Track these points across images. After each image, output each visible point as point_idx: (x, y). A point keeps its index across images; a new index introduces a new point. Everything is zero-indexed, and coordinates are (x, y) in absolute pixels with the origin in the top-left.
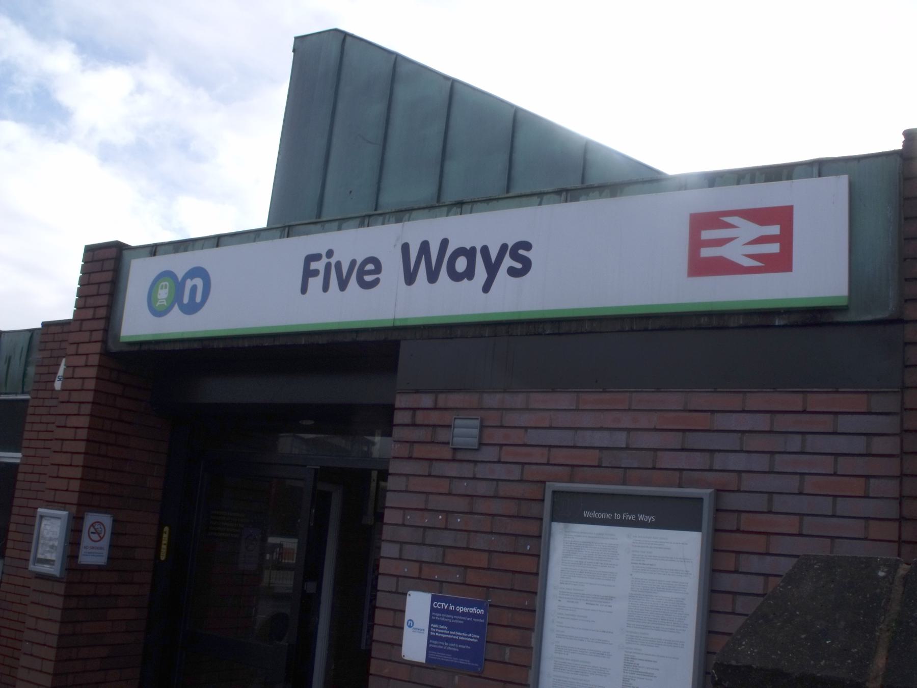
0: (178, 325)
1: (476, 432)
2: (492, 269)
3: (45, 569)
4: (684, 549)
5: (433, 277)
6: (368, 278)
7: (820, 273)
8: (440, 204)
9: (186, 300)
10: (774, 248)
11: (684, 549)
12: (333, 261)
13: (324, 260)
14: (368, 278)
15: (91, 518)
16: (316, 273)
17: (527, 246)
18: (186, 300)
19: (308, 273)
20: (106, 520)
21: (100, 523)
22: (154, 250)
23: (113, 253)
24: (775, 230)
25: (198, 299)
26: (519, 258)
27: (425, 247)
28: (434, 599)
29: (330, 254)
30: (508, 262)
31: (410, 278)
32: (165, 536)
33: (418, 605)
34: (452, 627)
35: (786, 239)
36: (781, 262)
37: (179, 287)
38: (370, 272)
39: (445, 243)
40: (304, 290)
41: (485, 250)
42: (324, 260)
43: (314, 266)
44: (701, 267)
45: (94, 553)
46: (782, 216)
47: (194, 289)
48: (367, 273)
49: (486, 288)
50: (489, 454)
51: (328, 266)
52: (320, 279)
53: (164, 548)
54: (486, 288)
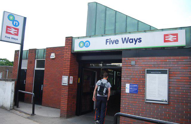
0: (84, 49)
1: (135, 63)
2: (136, 42)
3: (65, 85)
4: (165, 77)
5: (127, 42)
6: (117, 43)
7: (182, 42)
8: (126, 32)
9: (86, 45)
10: (175, 39)
11: (165, 77)
12: (111, 40)
13: (109, 40)
14: (117, 43)
15: (71, 77)
16: (108, 42)
17: (141, 38)
18: (86, 45)
19: (107, 42)
20: (72, 77)
21: (71, 77)
22: (79, 38)
23: (71, 38)
24: (175, 36)
25: (88, 45)
26: (140, 40)
27: (125, 38)
28: (130, 84)
29: (110, 39)
30: (138, 40)
31: (123, 43)
32: (42, 88)
33: (128, 86)
34: (133, 88)
35: (177, 38)
36: (177, 41)
37: (84, 44)
38: (117, 42)
39: (128, 38)
40: (106, 44)
41: (135, 39)
42: (109, 40)
43: (107, 41)
44: (165, 41)
45: (71, 82)
46: (177, 35)
47: (87, 44)
48: (116, 42)
49: (135, 44)
50: (136, 66)
51: (110, 41)
52: (109, 42)
53: (79, 81)
54: (135, 44)
